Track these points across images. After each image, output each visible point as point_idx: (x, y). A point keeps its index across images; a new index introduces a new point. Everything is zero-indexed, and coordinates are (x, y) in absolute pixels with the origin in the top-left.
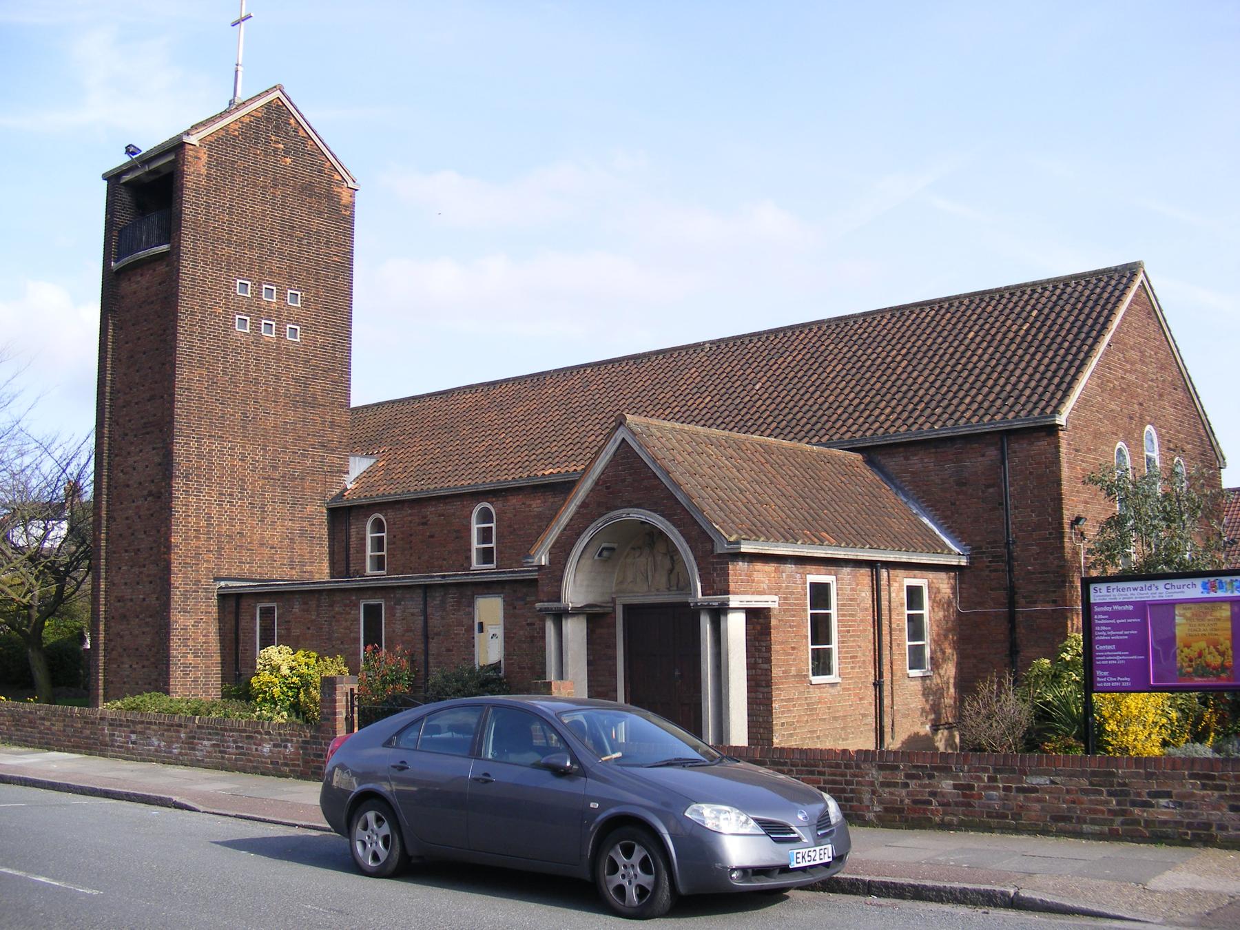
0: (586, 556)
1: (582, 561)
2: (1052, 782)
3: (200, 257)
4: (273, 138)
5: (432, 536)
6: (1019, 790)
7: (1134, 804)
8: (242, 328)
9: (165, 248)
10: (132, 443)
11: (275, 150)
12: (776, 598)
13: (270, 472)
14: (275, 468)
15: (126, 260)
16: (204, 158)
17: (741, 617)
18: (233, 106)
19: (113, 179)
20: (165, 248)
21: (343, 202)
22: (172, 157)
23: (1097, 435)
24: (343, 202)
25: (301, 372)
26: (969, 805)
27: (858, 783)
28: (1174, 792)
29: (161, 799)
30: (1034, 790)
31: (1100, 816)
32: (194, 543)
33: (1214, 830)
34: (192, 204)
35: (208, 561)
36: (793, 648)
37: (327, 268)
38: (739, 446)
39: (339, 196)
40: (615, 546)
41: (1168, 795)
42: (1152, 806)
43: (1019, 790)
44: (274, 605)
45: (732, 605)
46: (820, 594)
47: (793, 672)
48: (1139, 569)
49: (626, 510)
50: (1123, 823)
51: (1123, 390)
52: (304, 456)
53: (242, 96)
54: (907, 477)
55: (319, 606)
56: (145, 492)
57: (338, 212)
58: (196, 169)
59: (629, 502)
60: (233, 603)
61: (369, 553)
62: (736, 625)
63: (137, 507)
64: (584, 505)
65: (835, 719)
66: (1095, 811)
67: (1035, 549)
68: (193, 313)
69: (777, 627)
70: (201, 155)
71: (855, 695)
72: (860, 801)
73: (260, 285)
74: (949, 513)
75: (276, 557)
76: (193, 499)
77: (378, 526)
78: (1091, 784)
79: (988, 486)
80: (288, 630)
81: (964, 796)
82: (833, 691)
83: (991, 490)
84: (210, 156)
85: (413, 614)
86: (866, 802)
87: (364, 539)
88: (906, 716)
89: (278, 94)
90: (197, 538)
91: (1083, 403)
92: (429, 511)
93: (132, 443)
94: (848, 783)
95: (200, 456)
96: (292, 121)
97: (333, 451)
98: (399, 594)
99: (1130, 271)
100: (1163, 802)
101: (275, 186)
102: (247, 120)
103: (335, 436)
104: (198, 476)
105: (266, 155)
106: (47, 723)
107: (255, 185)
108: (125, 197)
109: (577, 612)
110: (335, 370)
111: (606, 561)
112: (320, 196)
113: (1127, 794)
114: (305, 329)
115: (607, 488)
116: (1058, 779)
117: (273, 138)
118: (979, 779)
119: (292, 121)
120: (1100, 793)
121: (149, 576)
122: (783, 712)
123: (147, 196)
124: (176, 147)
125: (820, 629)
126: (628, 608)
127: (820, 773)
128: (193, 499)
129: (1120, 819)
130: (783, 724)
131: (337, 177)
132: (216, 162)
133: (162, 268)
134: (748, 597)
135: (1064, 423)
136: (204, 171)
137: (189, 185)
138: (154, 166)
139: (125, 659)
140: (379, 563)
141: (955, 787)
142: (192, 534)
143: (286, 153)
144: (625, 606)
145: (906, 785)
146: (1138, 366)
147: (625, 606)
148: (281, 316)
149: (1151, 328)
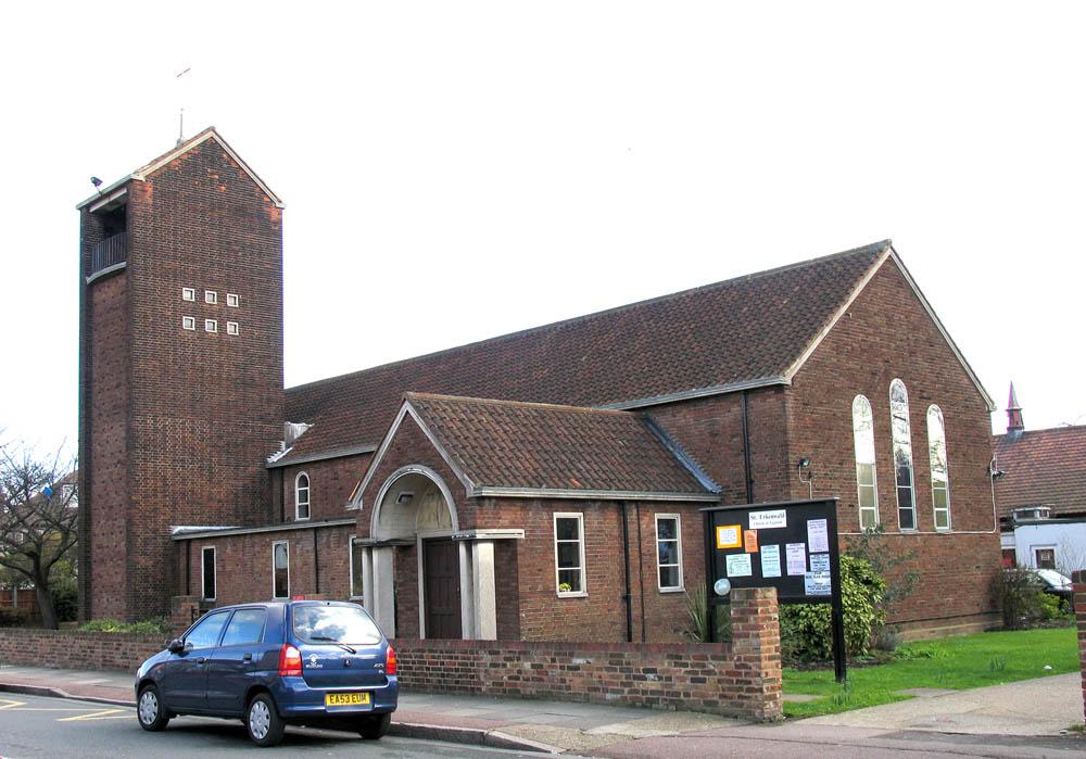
0: (388, 501)
1: (385, 506)
2: (588, 662)
3: (150, 271)
4: (209, 170)
5: (340, 489)
6: (570, 668)
7: (635, 678)
8: (188, 323)
9: (123, 264)
10: (105, 422)
11: (212, 180)
12: (522, 531)
13: (215, 440)
14: (220, 437)
15: (95, 275)
16: (150, 190)
17: (490, 547)
18: (181, 144)
19: (85, 209)
20: (123, 264)
21: (273, 219)
22: (125, 191)
23: (830, 390)
24: (273, 219)
25: (241, 359)
26: (542, 680)
27: (478, 665)
28: (659, 669)
29: (15, 687)
30: (577, 668)
31: (615, 688)
32: (152, 500)
33: (682, 697)
34: (139, 227)
35: (164, 514)
36: (540, 570)
37: (260, 274)
38: (513, 414)
39: (269, 216)
40: (412, 493)
41: (654, 671)
42: (646, 679)
43: (570, 668)
44: (214, 547)
45: (479, 536)
46: (568, 528)
47: (540, 588)
48: (589, 506)
49: (410, 466)
50: (629, 693)
51: (864, 351)
52: (245, 427)
53: (187, 136)
54: (674, 430)
55: (244, 547)
56: (116, 461)
57: (269, 228)
58: (144, 204)
59: (413, 459)
60: (183, 547)
61: (297, 504)
62: (485, 554)
63: (111, 473)
64: (383, 462)
65: (583, 625)
66: (613, 684)
67: (768, 487)
68: (146, 317)
69: (523, 554)
70: (146, 188)
71: (604, 607)
72: (478, 677)
73: (203, 291)
74: (705, 459)
75: (223, 509)
76: (150, 465)
77: (304, 481)
78: (610, 663)
79: (733, 437)
80: (223, 566)
81: (539, 673)
82: (582, 604)
83: (735, 440)
84: (155, 189)
85: (308, 551)
86: (482, 679)
87: (294, 492)
88: (657, 624)
89: (211, 134)
90: (155, 496)
91: (813, 364)
92: (340, 467)
93: (105, 422)
94: (472, 665)
95: (156, 430)
96: (225, 156)
97: (270, 423)
98: (298, 534)
99: (887, 243)
100: (651, 676)
101: (212, 210)
102: (185, 157)
103: (272, 409)
104: (155, 447)
105: (203, 185)
106: (6, 642)
107: (195, 210)
108: (95, 223)
109: (381, 545)
110: (269, 357)
111: (407, 504)
112: (252, 216)
113: (630, 670)
114: (242, 325)
115: (399, 449)
116: (590, 660)
117: (209, 170)
118: (545, 660)
119: (225, 156)
120: (615, 670)
121: (119, 527)
122: (530, 620)
123: (108, 221)
124: (128, 183)
125: (568, 555)
126: (427, 542)
127: (457, 658)
128: (150, 465)
129: (626, 690)
130: (530, 629)
131: (266, 199)
132: (160, 194)
133: (122, 281)
134: (495, 531)
135: (789, 382)
136: (150, 201)
137: (138, 213)
138: (113, 198)
139: (104, 594)
140: (305, 511)
141: (533, 666)
142: (150, 493)
143: (221, 182)
144: (423, 540)
145: (504, 666)
146: (884, 330)
147: (423, 540)
148: (222, 315)
149: (901, 296)
